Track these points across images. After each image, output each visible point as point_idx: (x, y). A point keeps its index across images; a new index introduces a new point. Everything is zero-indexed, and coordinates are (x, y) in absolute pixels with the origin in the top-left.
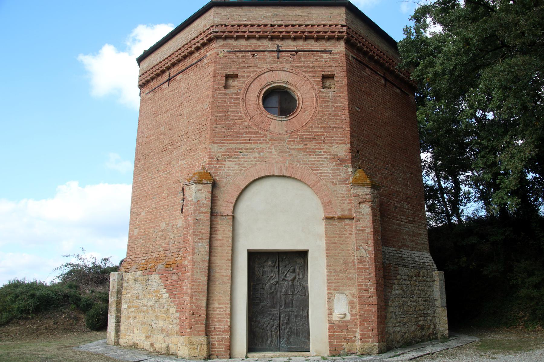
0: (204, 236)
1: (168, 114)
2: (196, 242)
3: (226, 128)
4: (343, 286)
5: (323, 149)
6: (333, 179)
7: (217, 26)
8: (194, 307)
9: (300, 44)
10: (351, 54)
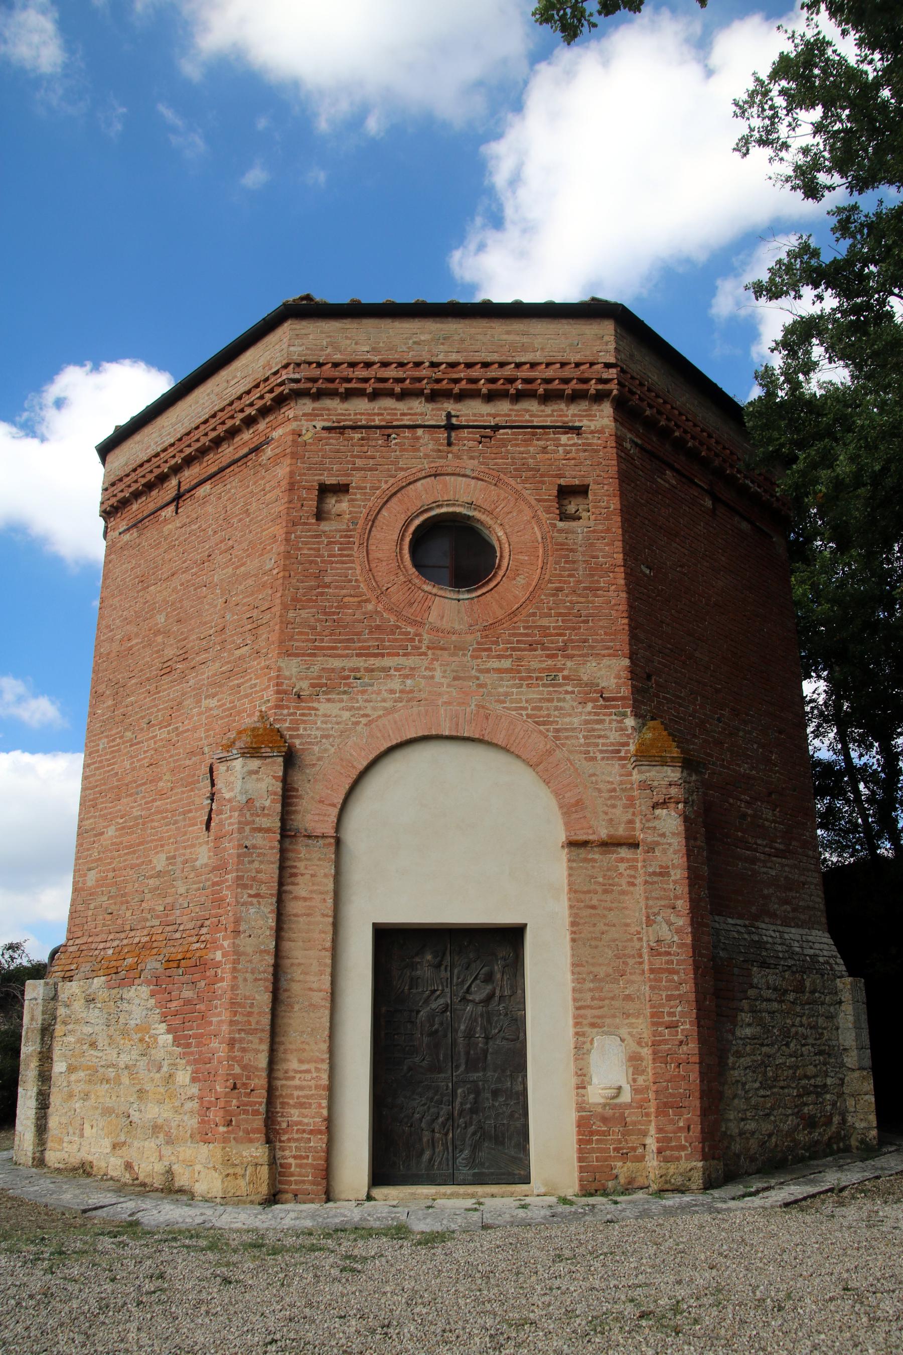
0: (264, 890)
1: (176, 582)
3: (319, 619)
4: (614, 1016)
5: (561, 670)
6: (588, 745)
7: (298, 365)
8: (237, 1070)
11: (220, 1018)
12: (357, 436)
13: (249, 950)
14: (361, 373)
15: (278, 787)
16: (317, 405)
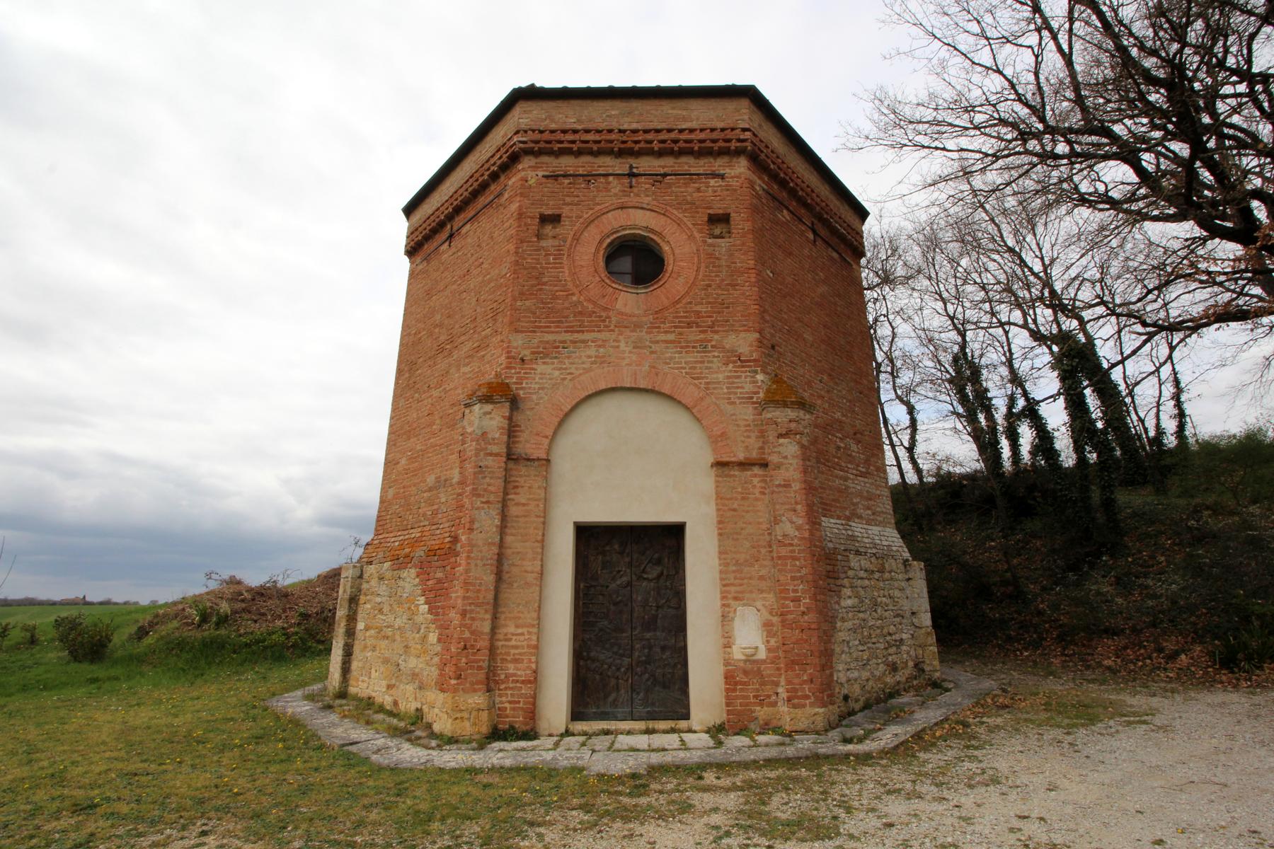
0: (492, 498)
1: (447, 292)
2: (478, 509)
3: (541, 308)
4: (751, 592)
6: (730, 393)
7: (526, 132)
8: (467, 635)
9: (666, 164)
10: (759, 182)
11: (457, 594)
12: (567, 181)
13: (480, 543)
14: (570, 137)
15: (505, 423)
16: (538, 160)
